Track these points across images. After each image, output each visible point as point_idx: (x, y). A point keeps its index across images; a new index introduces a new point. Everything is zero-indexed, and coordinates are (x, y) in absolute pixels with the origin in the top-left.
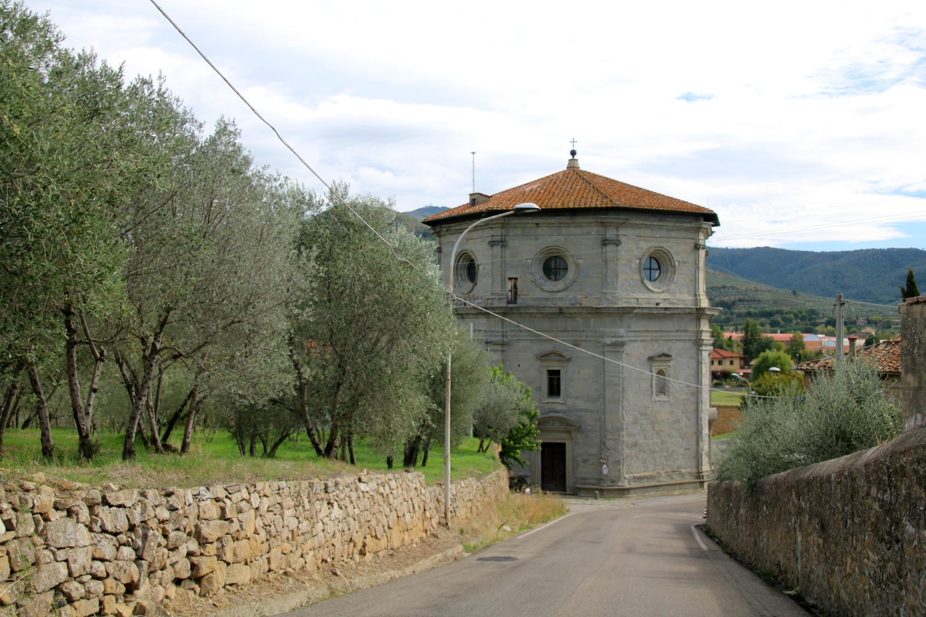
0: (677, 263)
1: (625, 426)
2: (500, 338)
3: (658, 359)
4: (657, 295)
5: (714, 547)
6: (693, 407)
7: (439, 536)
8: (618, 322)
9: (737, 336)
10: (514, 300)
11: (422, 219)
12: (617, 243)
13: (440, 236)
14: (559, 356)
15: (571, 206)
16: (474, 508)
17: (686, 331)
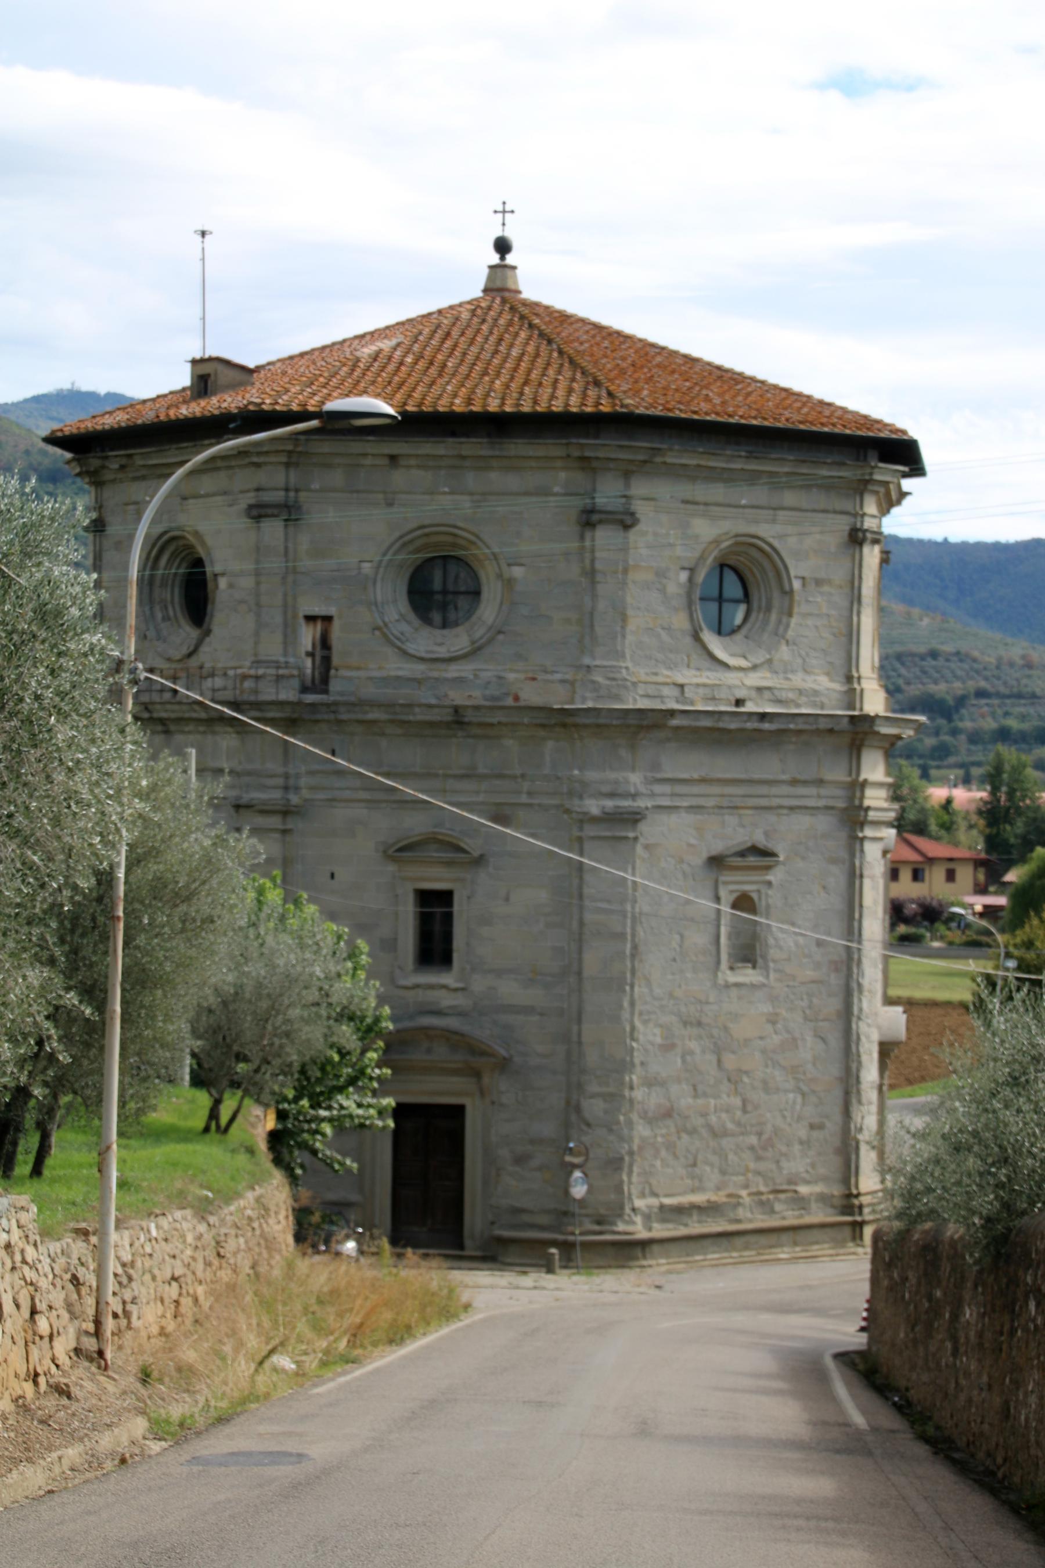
0: (797, 585)
1: (638, 1058)
2: (277, 794)
3: (738, 861)
4: (740, 675)
5: (889, 1419)
6: (835, 1004)
7: (75, 1391)
8: (623, 752)
9: (967, 797)
10: (322, 681)
11: (45, 429)
12: (626, 521)
13: (98, 483)
14: (451, 848)
15: (493, 406)
16: (186, 1302)
17: (820, 782)
